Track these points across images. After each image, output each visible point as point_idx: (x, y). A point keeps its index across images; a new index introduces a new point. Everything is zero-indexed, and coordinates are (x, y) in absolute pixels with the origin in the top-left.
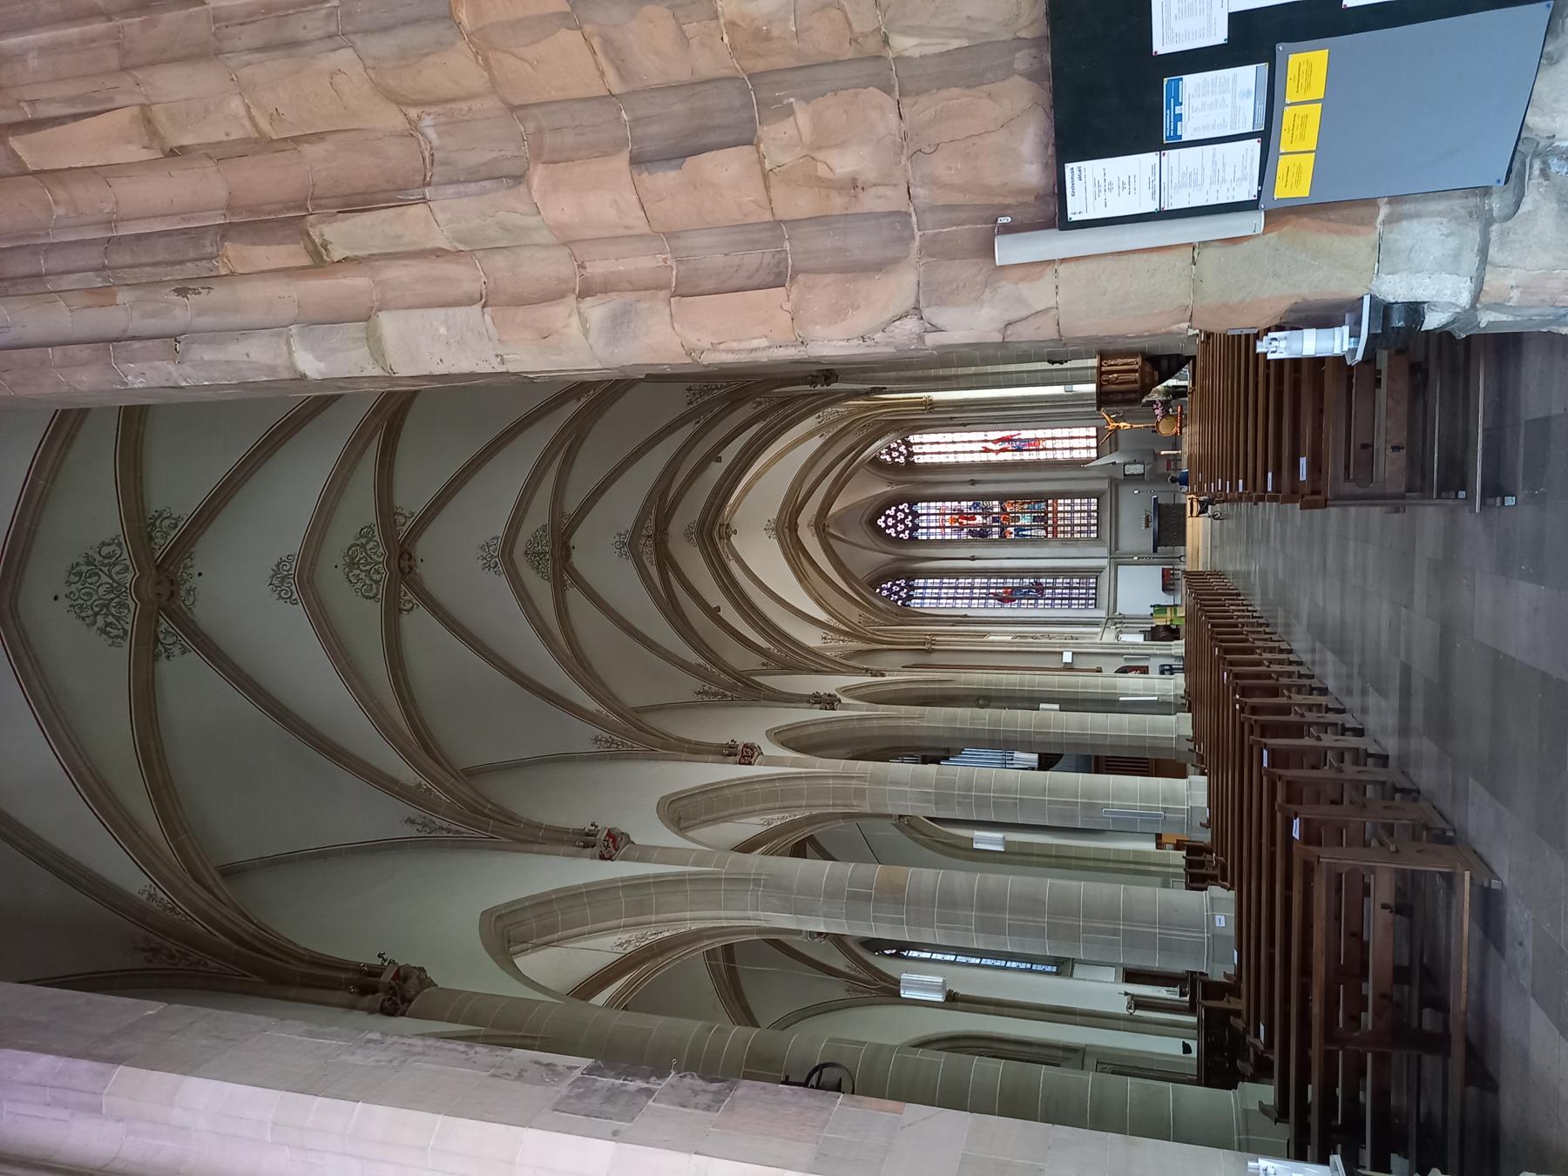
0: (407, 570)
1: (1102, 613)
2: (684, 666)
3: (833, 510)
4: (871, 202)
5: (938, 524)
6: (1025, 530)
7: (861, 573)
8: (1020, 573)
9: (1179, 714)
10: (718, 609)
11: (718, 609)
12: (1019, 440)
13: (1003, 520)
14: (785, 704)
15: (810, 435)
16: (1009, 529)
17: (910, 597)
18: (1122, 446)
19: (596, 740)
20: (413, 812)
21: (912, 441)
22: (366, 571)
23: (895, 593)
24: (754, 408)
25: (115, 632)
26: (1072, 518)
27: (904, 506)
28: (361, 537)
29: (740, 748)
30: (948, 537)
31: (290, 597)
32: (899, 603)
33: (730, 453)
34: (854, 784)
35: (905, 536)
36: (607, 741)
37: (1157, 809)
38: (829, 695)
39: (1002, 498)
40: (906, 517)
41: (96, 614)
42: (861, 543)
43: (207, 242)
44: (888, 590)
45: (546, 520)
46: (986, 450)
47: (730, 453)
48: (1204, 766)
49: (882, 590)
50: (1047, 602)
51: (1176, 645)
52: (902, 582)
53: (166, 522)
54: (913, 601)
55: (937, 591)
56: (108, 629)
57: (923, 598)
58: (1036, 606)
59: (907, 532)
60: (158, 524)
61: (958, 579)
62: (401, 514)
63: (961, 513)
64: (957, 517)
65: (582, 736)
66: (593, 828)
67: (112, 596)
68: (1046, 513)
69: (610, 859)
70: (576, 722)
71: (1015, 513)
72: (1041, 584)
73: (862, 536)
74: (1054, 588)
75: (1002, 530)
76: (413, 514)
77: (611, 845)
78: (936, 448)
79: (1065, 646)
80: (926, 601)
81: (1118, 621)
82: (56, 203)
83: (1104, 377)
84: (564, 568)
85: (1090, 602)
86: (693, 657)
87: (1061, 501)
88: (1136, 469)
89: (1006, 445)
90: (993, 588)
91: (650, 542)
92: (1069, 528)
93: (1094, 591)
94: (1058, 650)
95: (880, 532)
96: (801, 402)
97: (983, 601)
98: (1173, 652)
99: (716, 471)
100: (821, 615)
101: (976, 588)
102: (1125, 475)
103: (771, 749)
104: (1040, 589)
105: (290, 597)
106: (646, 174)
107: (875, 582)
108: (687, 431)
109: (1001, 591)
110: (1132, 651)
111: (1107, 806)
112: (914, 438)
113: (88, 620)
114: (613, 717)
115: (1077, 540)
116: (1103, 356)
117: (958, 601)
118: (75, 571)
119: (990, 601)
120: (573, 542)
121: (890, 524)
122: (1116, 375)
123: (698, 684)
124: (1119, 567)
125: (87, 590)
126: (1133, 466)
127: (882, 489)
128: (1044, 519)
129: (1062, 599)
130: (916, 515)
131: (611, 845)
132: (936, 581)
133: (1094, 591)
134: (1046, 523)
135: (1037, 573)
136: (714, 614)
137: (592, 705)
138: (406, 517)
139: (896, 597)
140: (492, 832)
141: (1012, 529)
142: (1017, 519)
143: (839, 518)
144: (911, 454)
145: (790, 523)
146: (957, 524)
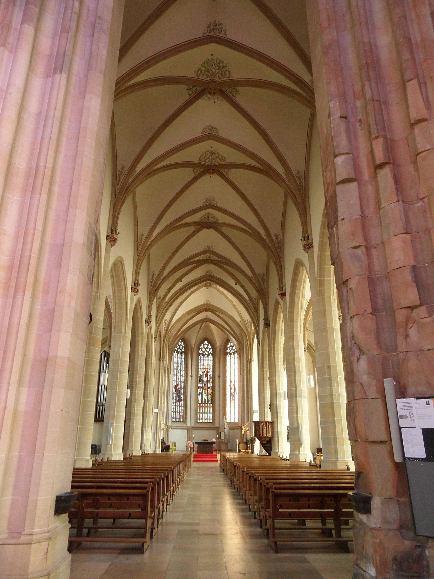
0: (209, 172)
1: (170, 424)
2: (164, 267)
3: (212, 325)
4: (400, 339)
5: (204, 363)
6: (201, 395)
7: (186, 336)
8: (185, 393)
9: (123, 455)
10: (181, 281)
11: (181, 281)
12: (234, 394)
13: (205, 387)
14: (148, 305)
15: (241, 317)
16: (202, 389)
17: (178, 352)
18: (231, 431)
19: (142, 235)
20: (126, 169)
21: (235, 354)
22: (209, 157)
23: (179, 347)
24: (254, 297)
25: (199, 73)
26: (205, 413)
27: (211, 351)
28: (222, 157)
29: (137, 288)
30: (199, 367)
31: (204, 132)
32: (176, 349)
33: (238, 288)
34: (123, 330)
35: (200, 351)
36: (141, 239)
37: (112, 442)
38: (151, 321)
39: (213, 388)
40: (207, 352)
41: (205, 67)
42: (199, 336)
43: (382, 133)
44: (181, 345)
45: (221, 221)
46: (231, 382)
47: (238, 288)
48: (97, 465)
49: (181, 342)
50: (175, 403)
51: (160, 451)
52: (183, 350)
53: (235, 93)
54: (176, 354)
55: (180, 363)
56: (200, 71)
57: (177, 357)
58: (173, 399)
59: (202, 352)
60: (234, 90)
61: (184, 370)
62: (228, 171)
63: (208, 372)
64: (207, 370)
65: (144, 230)
66: (117, 233)
67: (211, 73)
68: (207, 403)
69: (107, 239)
70: (149, 228)
71: (208, 392)
72: (181, 401)
73: (201, 335)
74: (180, 406)
75: (201, 387)
76: (228, 175)
77: (112, 239)
78: (232, 363)
79: (161, 410)
80: (176, 358)
81: (167, 431)
82: (390, 87)
83: (265, 423)
84: (202, 226)
85: (174, 419)
86: (166, 272)
87: (211, 408)
88: (223, 437)
89: (233, 389)
90: (180, 384)
91: (208, 258)
92: (201, 412)
93: (178, 421)
94: (159, 407)
95: (202, 342)
96: (255, 315)
97: (176, 380)
98: (157, 450)
99: (232, 282)
100: (174, 320)
101: (180, 377)
102: (221, 432)
103: (136, 298)
104: (179, 401)
105: (204, 132)
106: (410, 270)
107: (184, 340)
108: (249, 273)
109: (179, 386)
110: (158, 434)
111: (113, 423)
112: (236, 355)
113: (204, 64)
114: (150, 241)
115: (197, 415)
116: (272, 423)
117: (176, 370)
118: (221, 62)
119: (175, 382)
120: (211, 230)
121: (209, 349)
122: (265, 428)
123: (156, 273)
124: (186, 430)
125: (214, 65)
126: (224, 435)
127: (218, 344)
128: (205, 403)
129: (175, 409)
130: (208, 355)
131: (112, 239)
132: (184, 362)
133: (178, 421)
134: (204, 403)
135: (185, 400)
136: (180, 280)
137: (155, 234)
138: (227, 173)
139: (178, 348)
140: (118, 196)
141: (201, 391)
142: (205, 392)
143: (208, 327)
144: (230, 354)
145: (209, 309)
146: (204, 370)
